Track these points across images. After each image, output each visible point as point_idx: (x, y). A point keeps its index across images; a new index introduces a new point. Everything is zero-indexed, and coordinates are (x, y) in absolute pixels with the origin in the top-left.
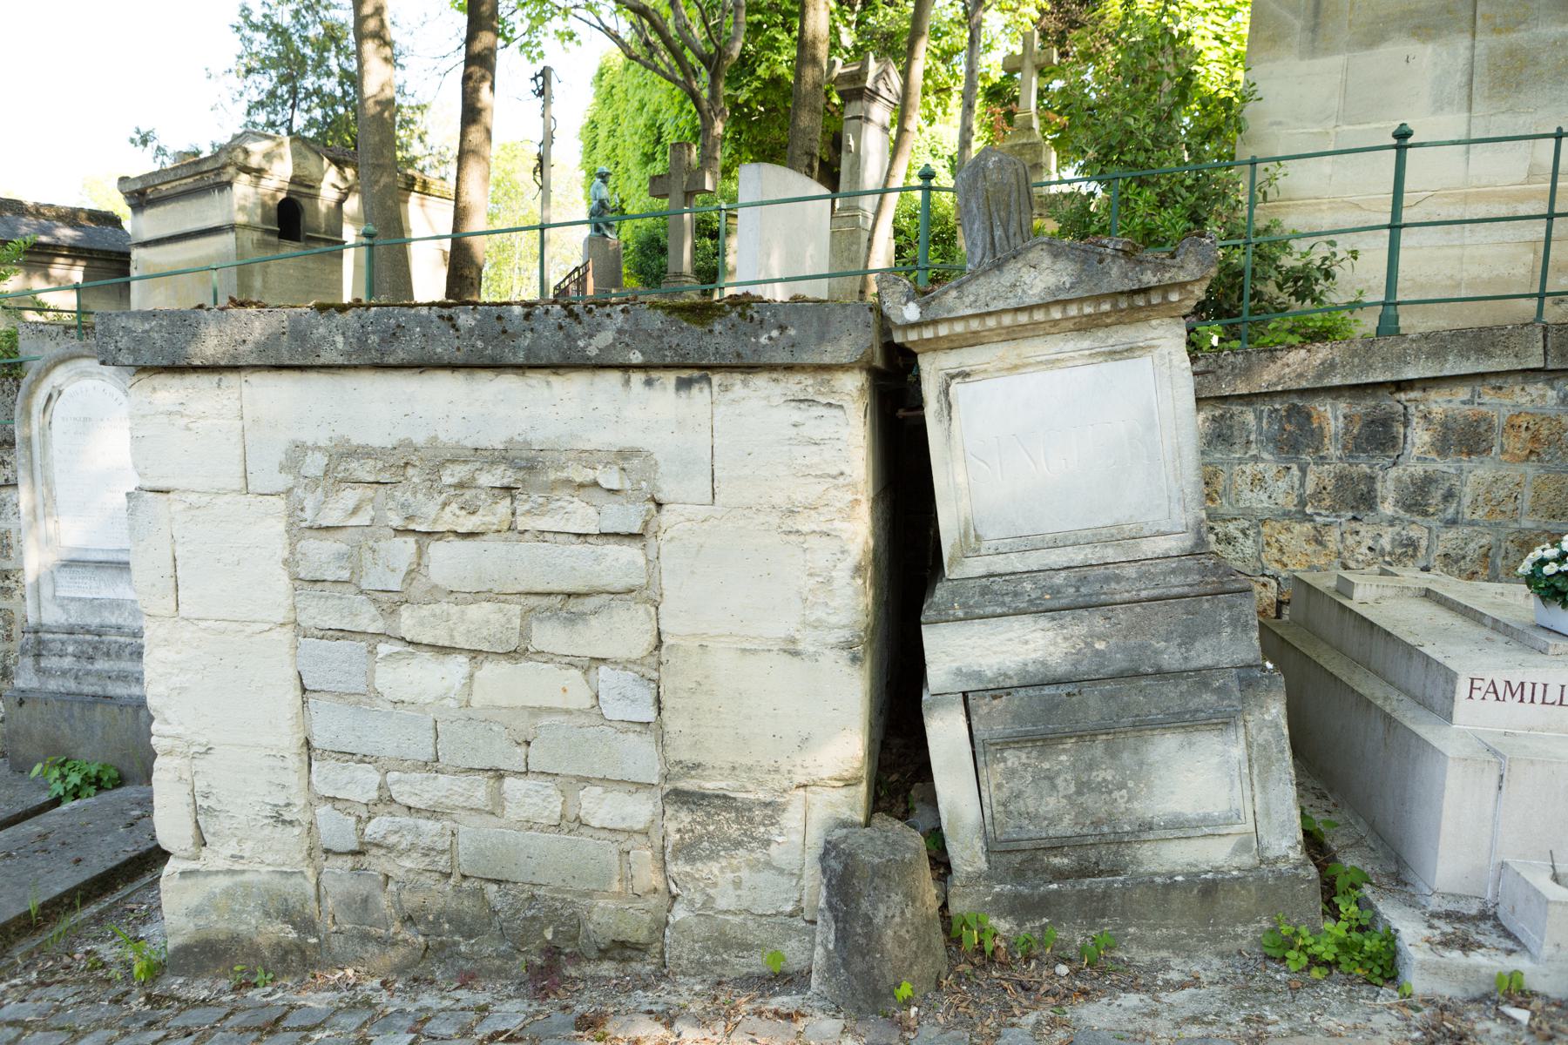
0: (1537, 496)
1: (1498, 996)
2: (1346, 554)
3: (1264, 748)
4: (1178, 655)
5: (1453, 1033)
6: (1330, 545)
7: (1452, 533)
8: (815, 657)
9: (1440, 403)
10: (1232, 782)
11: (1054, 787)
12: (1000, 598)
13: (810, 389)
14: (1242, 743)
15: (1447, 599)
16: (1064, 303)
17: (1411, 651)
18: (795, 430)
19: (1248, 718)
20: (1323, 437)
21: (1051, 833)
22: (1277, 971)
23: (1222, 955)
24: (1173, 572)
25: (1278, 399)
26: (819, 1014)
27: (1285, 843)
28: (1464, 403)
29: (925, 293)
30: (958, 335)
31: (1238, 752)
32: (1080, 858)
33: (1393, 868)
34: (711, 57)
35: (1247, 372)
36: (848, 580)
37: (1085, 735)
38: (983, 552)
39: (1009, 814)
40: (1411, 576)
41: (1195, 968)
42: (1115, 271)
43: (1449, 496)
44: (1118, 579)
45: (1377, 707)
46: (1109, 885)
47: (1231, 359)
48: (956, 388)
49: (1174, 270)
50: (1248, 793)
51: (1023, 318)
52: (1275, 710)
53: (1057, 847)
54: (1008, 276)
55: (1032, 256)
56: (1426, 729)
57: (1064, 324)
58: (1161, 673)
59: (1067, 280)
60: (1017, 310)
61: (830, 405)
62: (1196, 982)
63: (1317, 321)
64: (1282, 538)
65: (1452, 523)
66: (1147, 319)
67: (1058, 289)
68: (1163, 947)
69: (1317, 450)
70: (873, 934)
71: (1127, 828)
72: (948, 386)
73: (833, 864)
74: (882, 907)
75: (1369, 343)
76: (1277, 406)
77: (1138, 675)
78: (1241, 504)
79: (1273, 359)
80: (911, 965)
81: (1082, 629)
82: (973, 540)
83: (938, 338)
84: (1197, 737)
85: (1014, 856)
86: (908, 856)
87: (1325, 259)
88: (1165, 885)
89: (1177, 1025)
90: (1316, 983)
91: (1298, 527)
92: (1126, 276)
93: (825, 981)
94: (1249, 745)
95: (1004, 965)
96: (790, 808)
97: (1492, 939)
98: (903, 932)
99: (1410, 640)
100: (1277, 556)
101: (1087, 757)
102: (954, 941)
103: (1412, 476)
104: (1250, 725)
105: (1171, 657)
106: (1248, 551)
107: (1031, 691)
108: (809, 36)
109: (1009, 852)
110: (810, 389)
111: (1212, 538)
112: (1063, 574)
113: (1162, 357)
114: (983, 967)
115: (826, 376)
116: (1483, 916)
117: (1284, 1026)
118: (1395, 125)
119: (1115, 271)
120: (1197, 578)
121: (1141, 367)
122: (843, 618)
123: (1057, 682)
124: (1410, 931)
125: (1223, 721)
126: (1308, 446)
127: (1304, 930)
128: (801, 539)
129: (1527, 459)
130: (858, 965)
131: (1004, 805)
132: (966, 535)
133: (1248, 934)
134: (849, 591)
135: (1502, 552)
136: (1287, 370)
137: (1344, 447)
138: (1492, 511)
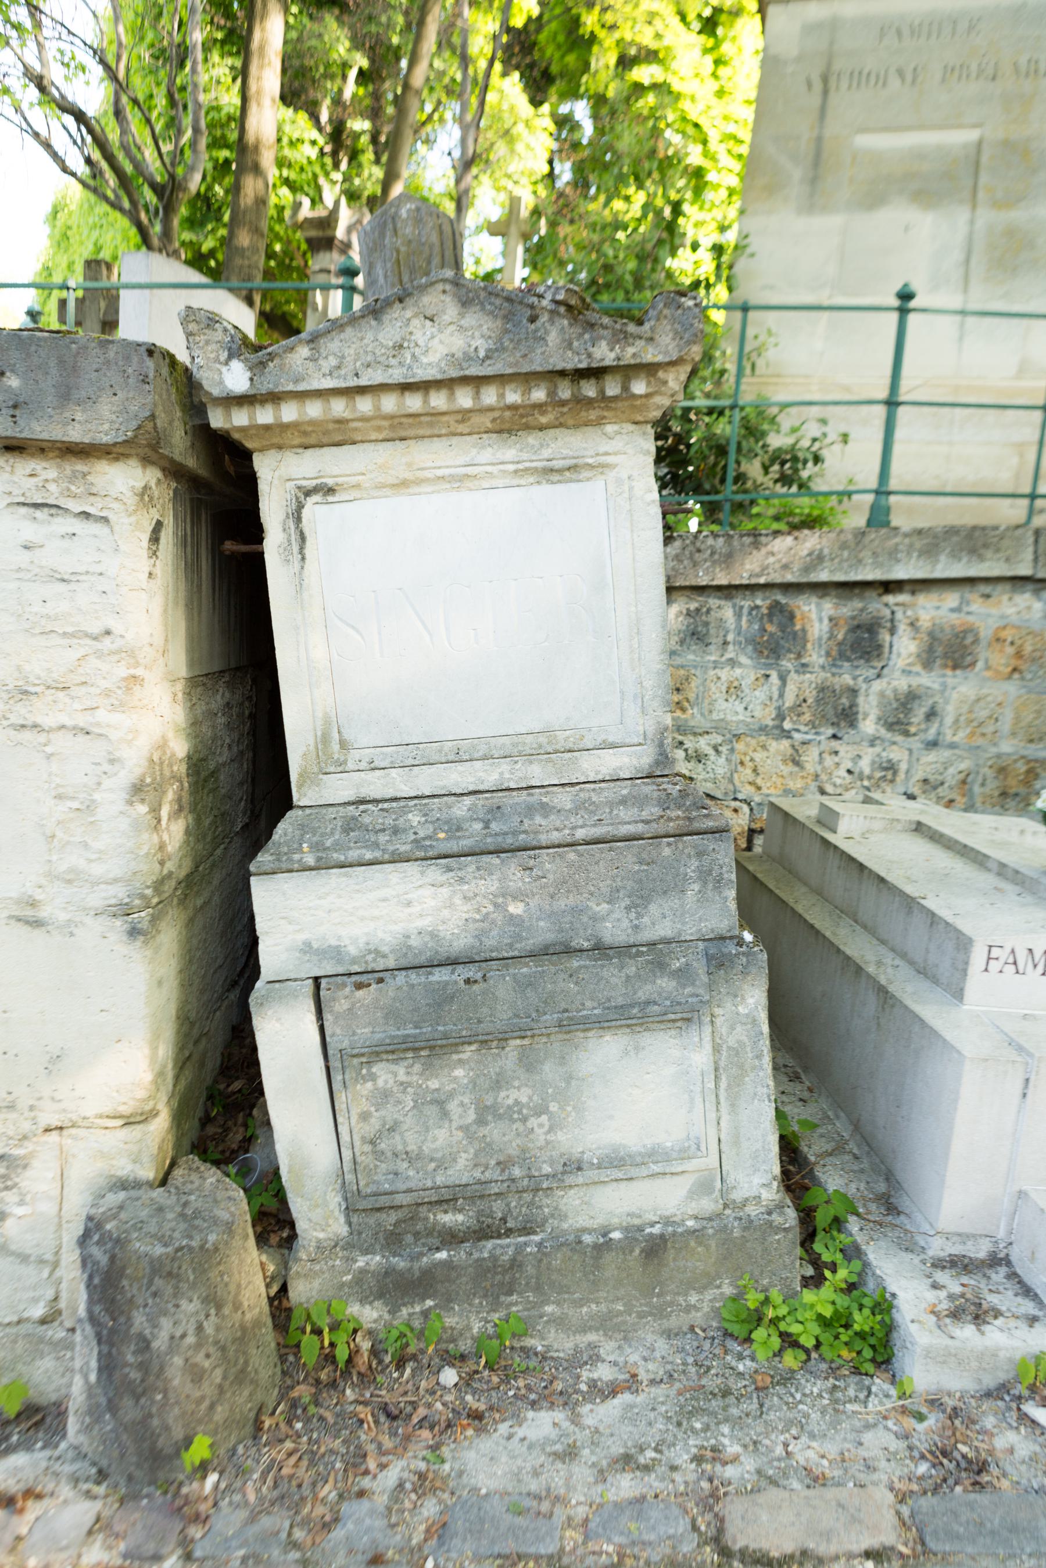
0: (1017, 719)
1: (1021, 1389)
2: (824, 777)
3: (736, 1052)
4: (625, 923)
5: (970, 1462)
6: (808, 766)
7: (932, 756)
8: (69, 929)
9: (932, 610)
10: (692, 1100)
11: (445, 1114)
12: (375, 836)
13: (52, 487)
14: (708, 1047)
15: (942, 835)
16: (478, 382)
17: (910, 904)
18: (27, 555)
19: (717, 1011)
20: (805, 641)
21: (440, 1180)
22: (740, 1357)
23: (668, 1334)
24: (623, 801)
25: (759, 594)
26: (66, 1491)
27: (758, 1180)
28: (952, 610)
29: (258, 348)
30: (312, 422)
31: (701, 1058)
32: (480, 1213)
33: (882, 1187)
34: (163, 187)
35: (728, 559)
36: (121, 806)
37: (489, 1041)
38: (350, 766)
39: (379, 1155)
40: (895, 805)
41: (632, 1359)
42: (553, 337)
43: (932, 714)
44: (545, 809)
45: (869, 976)
46: (520, 1249)
47: (710, 541)
48: (314, 510)
49: (640, 343)
50: (712, 1116)
51: (414, 402)
52: (753, 1000)
53: (447, 1201)
54: (390, 329)
55: (431, 300)
56: (929, 1008)
57: (477, 419)
58: (600, 949)
59: (482, 345)
60: (406, 387)
61: (86, 515)
62: (632, 1383)
63: (804, 504)
64: (759, 756)
65: (933, 744)
66: (599, 422)
67: (467, 357)
68: (590, 1328)
69: (799, 656)
70: (151, 1367)
71: (547, 1169)
72: (300, 507)
73: (96, 1252)
74: (166, 1323)
75: (860, 535)
76: (759, 602)
77: (569, 951)
78: (715, 716)
79: (756, 545)
80: (212, 1407)
81: (492, 885)
82: (336, 747)
83: (284, 427)
84: (647, 1039)
85: (386, 1218)
86: (212, 1238)
87: (814, 440)
88: (597, 1247)
89: (602, 1476)
90: (787, 1378)
91: (774, 744)
92: (570, 344)
93: (87, 1429)
94: (716, 1049)
95: (366, 1379)
96: (35, 1163)
97: (1006, 1300)
98: (199, 1358)
99: (909, 889)
100: (751, 777)
101: (493, 1070)
102: (288, 1351)
103: (895, 690)
104: (719, 1021)
105: (615, 927)
106: (720, 771)
107: (413, 975)
108: (251, 137)
109: (379, 1210)
110: (52, 487)
111: (680, 754)
112: (468, 801)
113: (619, 481)
114: (333, 1384)
115: (80, 466)
116: (995, 1261)
117: (749, 1464)
118: (897, 287)
119: (553, 337)
120: (656, 811)
121: (584, 497)
122: (115, 867)
123: (453, 962)
124: (913, 1296)
125: (684, 1016)
126: (789, 651)
127: (776, 1296)
128: (42, 738)
129: (1009, 677)
130: (130, 1411)
131: (372, 1142)
132: (325, 739)
133: (703, 1304)
134: (124, 824)
135: (980, 779)
136: (771, 560)
137: (828, 654)
138: (972, 734)
